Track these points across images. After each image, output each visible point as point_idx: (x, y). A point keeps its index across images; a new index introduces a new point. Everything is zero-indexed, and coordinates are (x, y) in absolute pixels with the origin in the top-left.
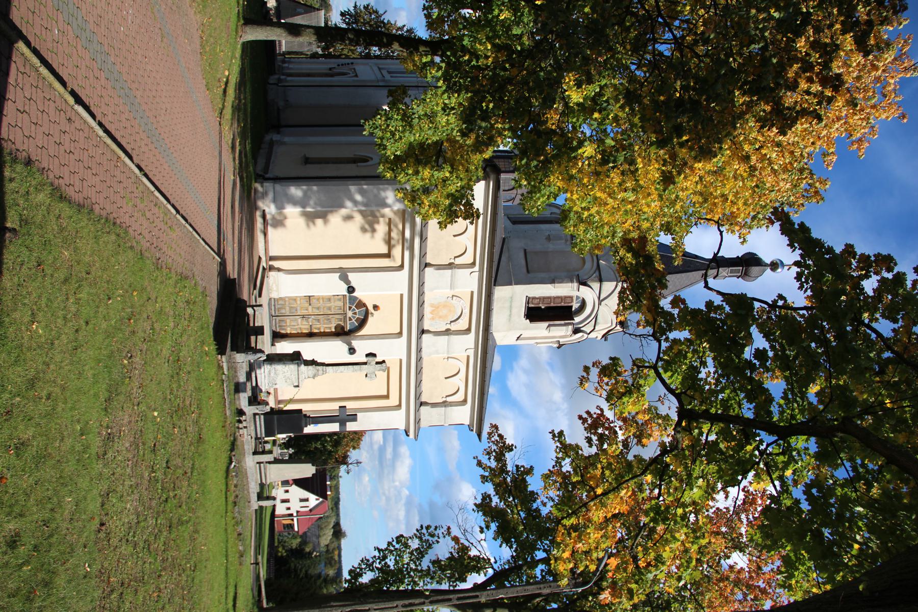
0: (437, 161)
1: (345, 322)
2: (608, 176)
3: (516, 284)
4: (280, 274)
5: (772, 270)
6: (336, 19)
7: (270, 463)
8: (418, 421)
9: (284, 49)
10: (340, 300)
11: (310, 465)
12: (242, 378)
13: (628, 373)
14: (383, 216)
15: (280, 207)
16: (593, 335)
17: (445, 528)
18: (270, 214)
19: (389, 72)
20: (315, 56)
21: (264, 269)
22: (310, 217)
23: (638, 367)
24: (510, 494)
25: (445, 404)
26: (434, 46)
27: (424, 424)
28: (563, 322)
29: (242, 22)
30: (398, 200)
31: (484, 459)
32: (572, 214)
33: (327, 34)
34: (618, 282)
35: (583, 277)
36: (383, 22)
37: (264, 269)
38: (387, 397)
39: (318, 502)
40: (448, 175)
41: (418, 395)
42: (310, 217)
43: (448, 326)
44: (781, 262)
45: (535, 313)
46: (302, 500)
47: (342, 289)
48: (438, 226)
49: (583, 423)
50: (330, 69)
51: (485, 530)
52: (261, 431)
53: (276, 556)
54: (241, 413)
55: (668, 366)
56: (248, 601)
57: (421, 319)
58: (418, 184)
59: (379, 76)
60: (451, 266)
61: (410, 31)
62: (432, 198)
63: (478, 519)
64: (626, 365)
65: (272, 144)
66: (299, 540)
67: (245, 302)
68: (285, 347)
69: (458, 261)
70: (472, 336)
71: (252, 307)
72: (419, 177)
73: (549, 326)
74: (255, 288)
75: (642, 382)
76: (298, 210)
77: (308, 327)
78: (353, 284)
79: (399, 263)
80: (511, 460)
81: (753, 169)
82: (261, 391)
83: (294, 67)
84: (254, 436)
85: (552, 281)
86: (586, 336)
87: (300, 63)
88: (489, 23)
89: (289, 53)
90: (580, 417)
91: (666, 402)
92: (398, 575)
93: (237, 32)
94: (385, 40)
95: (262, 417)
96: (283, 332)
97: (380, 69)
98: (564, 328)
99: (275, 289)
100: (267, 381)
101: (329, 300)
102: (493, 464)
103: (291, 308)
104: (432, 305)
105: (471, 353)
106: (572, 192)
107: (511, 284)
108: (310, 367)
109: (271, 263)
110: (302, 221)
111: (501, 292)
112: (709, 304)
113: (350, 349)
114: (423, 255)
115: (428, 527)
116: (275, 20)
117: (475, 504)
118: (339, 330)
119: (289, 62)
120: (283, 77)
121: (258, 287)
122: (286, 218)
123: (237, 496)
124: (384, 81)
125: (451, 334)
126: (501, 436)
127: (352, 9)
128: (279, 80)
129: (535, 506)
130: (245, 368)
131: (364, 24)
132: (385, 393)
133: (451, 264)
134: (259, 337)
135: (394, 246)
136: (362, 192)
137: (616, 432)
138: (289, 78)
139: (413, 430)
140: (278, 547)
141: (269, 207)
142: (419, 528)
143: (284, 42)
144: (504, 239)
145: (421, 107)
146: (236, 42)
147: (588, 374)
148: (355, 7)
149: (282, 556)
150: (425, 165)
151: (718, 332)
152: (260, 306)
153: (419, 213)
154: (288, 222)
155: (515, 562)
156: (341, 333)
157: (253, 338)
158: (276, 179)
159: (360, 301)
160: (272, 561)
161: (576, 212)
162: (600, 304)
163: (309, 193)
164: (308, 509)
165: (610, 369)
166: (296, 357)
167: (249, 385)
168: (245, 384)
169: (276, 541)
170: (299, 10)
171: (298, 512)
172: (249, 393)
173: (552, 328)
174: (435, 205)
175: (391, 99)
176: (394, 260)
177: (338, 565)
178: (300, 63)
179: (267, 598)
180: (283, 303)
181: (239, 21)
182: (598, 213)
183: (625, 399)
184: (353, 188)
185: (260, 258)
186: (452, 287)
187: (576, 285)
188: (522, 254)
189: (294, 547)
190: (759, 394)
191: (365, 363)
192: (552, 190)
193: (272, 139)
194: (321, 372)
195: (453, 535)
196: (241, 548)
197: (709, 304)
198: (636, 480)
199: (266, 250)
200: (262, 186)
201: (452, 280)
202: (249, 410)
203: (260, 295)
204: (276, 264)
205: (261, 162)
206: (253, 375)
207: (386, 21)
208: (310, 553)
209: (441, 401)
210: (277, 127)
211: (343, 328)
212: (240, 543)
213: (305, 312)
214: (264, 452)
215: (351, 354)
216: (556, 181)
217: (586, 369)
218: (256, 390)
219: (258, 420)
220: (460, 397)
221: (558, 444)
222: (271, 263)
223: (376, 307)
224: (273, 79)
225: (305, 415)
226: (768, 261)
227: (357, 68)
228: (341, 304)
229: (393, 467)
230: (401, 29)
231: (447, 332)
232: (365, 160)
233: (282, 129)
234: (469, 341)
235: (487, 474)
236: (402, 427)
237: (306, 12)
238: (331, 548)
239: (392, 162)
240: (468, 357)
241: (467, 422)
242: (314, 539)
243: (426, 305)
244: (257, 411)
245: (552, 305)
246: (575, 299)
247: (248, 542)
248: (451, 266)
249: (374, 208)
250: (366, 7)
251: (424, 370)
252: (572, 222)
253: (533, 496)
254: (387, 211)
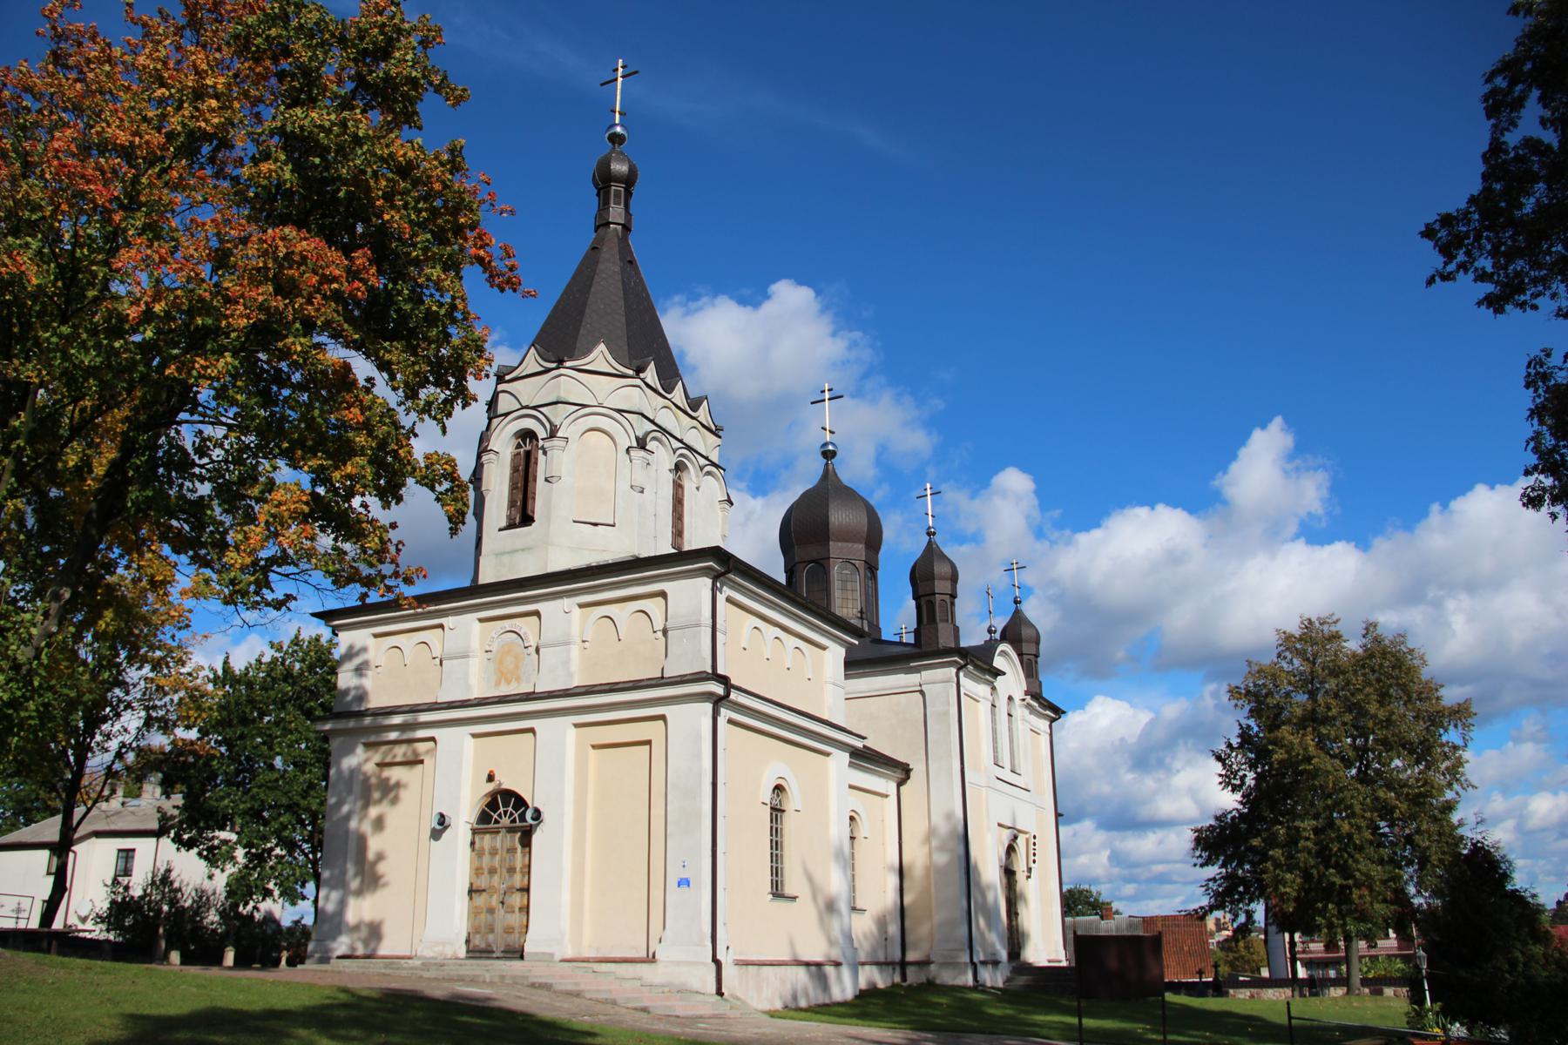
22: (372, 880)
42: (372, 880)
99: (441, 948)
201: (456, 658)
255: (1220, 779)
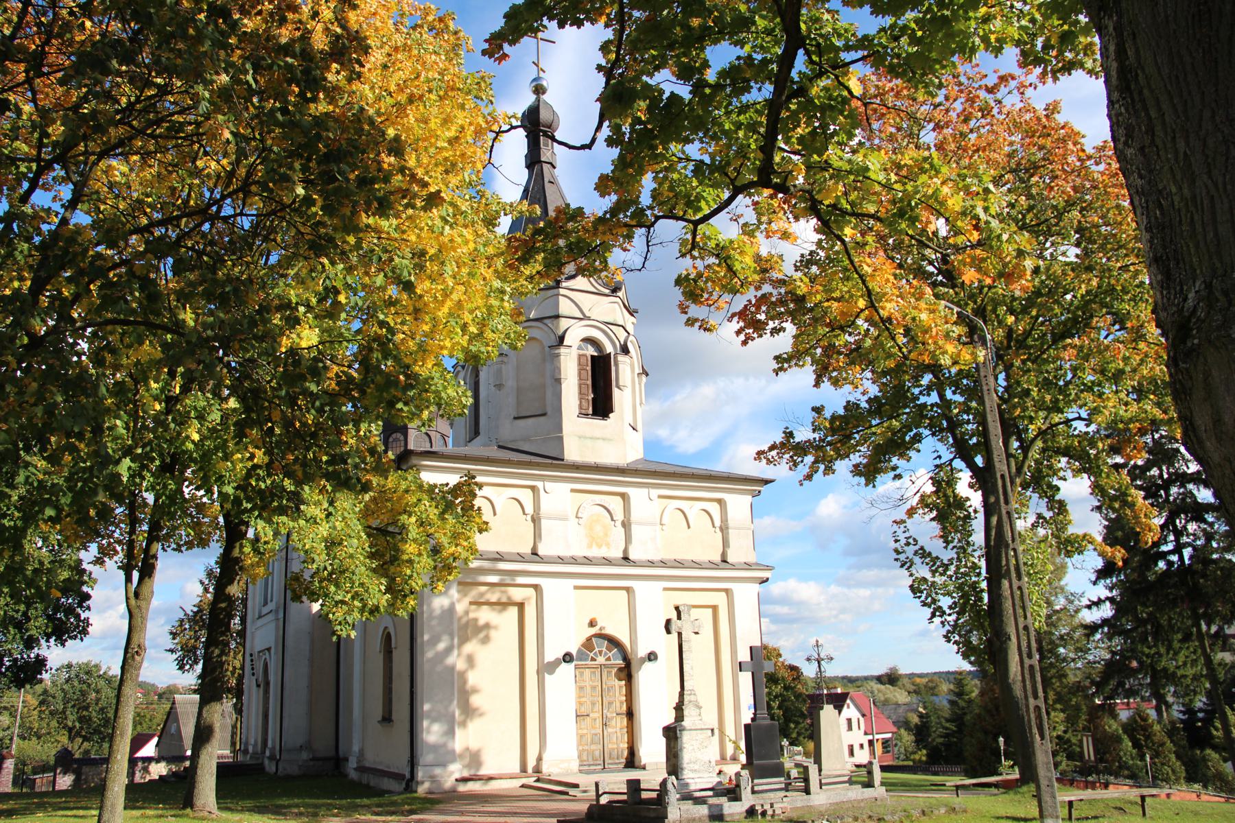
0: (393, 534)
1: (612, 666)
2: (421, 297)
3: (561, 430)
4: (545, 757)
5: (544, 93)
6: (190, 678)
7: (820, 770)
8: (748, 566)
9: (227, 752)
10: (582, 674)
11: (822, 712)
12: (703, 810)
13: (699, 263)
14: (467, 613)
15: (452, 756)
16: (630, 328)
17: (895, 527)
18: (461, 771)
19: (266, 603)
20: (238, 709)
21: (538, 780)
22: (469, 712)
23: (693, 248)
24: (849, 437)
25: (724, 529)
26: (234, 533)
27: (752, 558)
28: (613, 368)
29: (188, 811)
30: (448, 589)
31: (803, 469)
32: (473, 349)
33: (210, 690)
34: (558, 295)
35: (554, 341)
36: (196, 613)
37: (538, 780)
38: (715, 608)
39: (851, 706)
40: (413, 519)
41: (713, 565)
42: (469, 712)
43: (619, 524)
44: (534, 80)
45: (601, 405)
46: (850, 728)
47: (567, 670)
48: (485, 533)
49: (753, 339)
50: (258, 686)
51: (898, 472)
52: (778, 782)
53: (926, 763)
54: (751, 812)
55: (692, 203)
56: (1011, 801)
57: (608, 562)
58: (426, 561)
59: (271, 617)
60: (536, 520)
61: (210, 574)
62: (445, 541)
63: (885, 484)
64: (686, 266)
65: (361, 769)
66: (902, 731)
67: (591, 807)
68: (652, 750)
69: (530, 509)
70: (631, 491)
71: (598, 796)
72: (417, 559)
73: (618, 387)
74: (567, 793)
75: (712, 244)
76: (459, 732)
77: (619, 718)
78: (560, 655)
79: (531, 591)
80: (804, 434)
81: (411, 100)
82: (720, 783)
83: (254, 736)
84: (783, 793)
85: (558, 381)
86: (631, 338)
87: (248, 729)
88: (206, 456)
89: (233, 744)
90: (745, 343)
91: (739, 212)
92: (967, 594)
93: (203, 819)
94: (223, 605)
95: (756, 781)
96: (626, 753)
97: (260, 617)
98: (621, 366)
100: (706, 775)
101: (581, 688)
102: (809, 459)
103: (592, 743)
104: (590, 546)
105: (655, 492)
106: (442, 348)
107: (561, 438)
108: (686, 713)
109: (530, 770)
110: (474, 725)
111: (572, 452)
112: (610, 142)
113: (650, 660)
114: (521, 558)
115: (897, 552)
116: (187, 763)
117: (867, 485)
118: (623, 675)
119: (247, 744)
120: (268, 753)
121: (566, 788)
122: (468, 749)
123: (870, 817)
124: (277, 611)
125: (629, 520)
126: (772, 448)
127: (175, 656)
128: (272, 758)
129: (864, 405)
130: (688, 806)
131: (197, 639)
132: (710, 611)
133: (533, 520)
134: (643, 786)
135: (509, 598)
136: (435, 640)
137: (764, 296)
138: (270, 744)
139: (759, 572)
140: (914, 761)
141: (452, 773)
142: (899, 564)
143: (217, 751)
144: (500, 447)
145: (316, 557)
146: (218, 819)
147: (696, 320)
148: (172, 651)
149: (928, 755)
150: (397, 550)
151: (652, 130)
152: (597, 785)
153: (466, 560)
154: (474, 746)
155: (942, 430)
156: (627, 672)
157: (645, 795)
158: (413, 763)
159: (584, 645)
160: (936, 768)
161: (470, 341)
162: (589, 318)
163: (434, 714)
164: (862, 720)
165: (691, 289)
166: (672, 734)
167: (712, 801)
168: (710, 806)
169: (906, 763)
170: (173, 730)
171: (866, 733)
172: (723, 800)
173: (621, 383)
174: (455, 537)
175: (304, 598)
176: (529, 599)
177: (936, 678)
178: (248, 729)
179: (992, 775)
180: (585, 754)
181: (187, 815)
182: (471, 312)
183: (737, 266)
184: (430, 654)
185: (523, 786)
186: (565, 519)
187: (562, 350)
188: (521, 423)
189: (913, 738)
190: (737, 77)
191: (680, 634)
192: (438, 375)
193: (355, 769)
194: (692, 698)
195: (905, 517)
196: (943, 811)
197: (610, 142)
198: (852, 252)
199: (512, 777)
200: (423, 783)
201: (555, 519)
202: (748, 799)
203: (576, 786)
204: (531, 763)
205: (387, 784)
206: (698, 794)
207: (195, 609)
208: (921, 716)
209: (719, 534)
210: (338, 761)
211: (620, 670)
212: (936, 812)
213: (599, 723)
214: (806, 780)
215: (656, 658)
216: (424, 369)
217: (690, 322)
218: (718, 791)
219: (760, 788)
220: (714, 508)
221: (793, 363)
222: (530, 770)
223: (592, 624)
224: (270, 767)
225: (753, 720)
226: (533, 98)
227: (257, 648)
228: (587, 672)
229: (800, 604)
230: (206, 590)
231: (626, 525)
232: (387, 638)
233: (341, 754)
234: (638, 495)
235: (822, 467)
236: (756, 587)
237: (177, 720)
238: (912, 688)
239: (395, 598)
240: (660, 497)
241: (749, 498)
242: (901, 710)
243: (589, 554)
244: (749, 789)
245: (589, 382)
246: (582, 352)
247: (933, 801)
248: (536, 520)
249: (456, 626)
250: (174, 635)
251: (679, 557)
252: (483, 349)
253: (851, 407)
254: (460, 608)
255: (1050, 80)
